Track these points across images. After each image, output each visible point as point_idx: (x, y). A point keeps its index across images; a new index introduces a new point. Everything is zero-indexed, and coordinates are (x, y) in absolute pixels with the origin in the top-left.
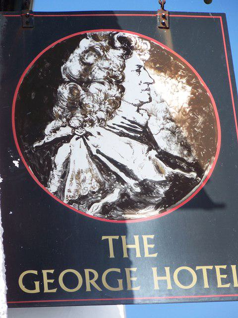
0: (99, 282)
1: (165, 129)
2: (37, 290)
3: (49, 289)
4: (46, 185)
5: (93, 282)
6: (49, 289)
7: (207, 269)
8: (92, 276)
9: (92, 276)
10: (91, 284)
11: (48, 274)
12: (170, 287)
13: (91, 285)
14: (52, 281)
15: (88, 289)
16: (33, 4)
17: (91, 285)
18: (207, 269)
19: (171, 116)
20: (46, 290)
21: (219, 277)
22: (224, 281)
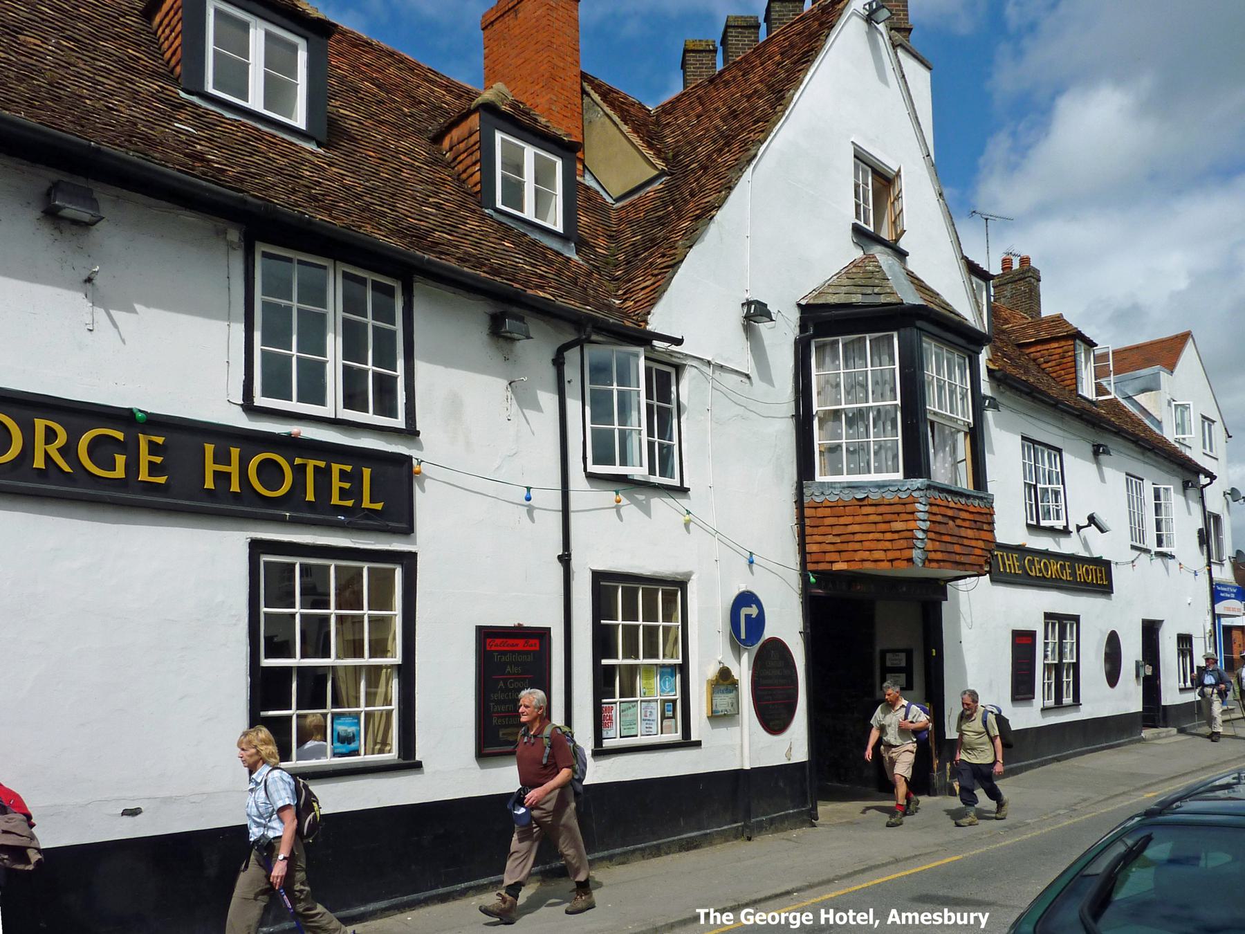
0: (68, 451)
1: (1153, 553)
2: (119, 473)
3: (341, 499)
4: (346, 276)
5: (53, 450)
6: (341, 499)
7: (340, 469)
8: (50, 435)
9: (50, 435)
10: (46, 452)
11: (342, 472)
12: (235, 487)
13: (47, 456)
14: (347, 485)
15: (39, 463)
16: (1154, 468)
17: (47, 456)
18: (340, 469)
19: (583, 168)
20: (143, 476)
21: (336, 484)
22: (344, 494)
